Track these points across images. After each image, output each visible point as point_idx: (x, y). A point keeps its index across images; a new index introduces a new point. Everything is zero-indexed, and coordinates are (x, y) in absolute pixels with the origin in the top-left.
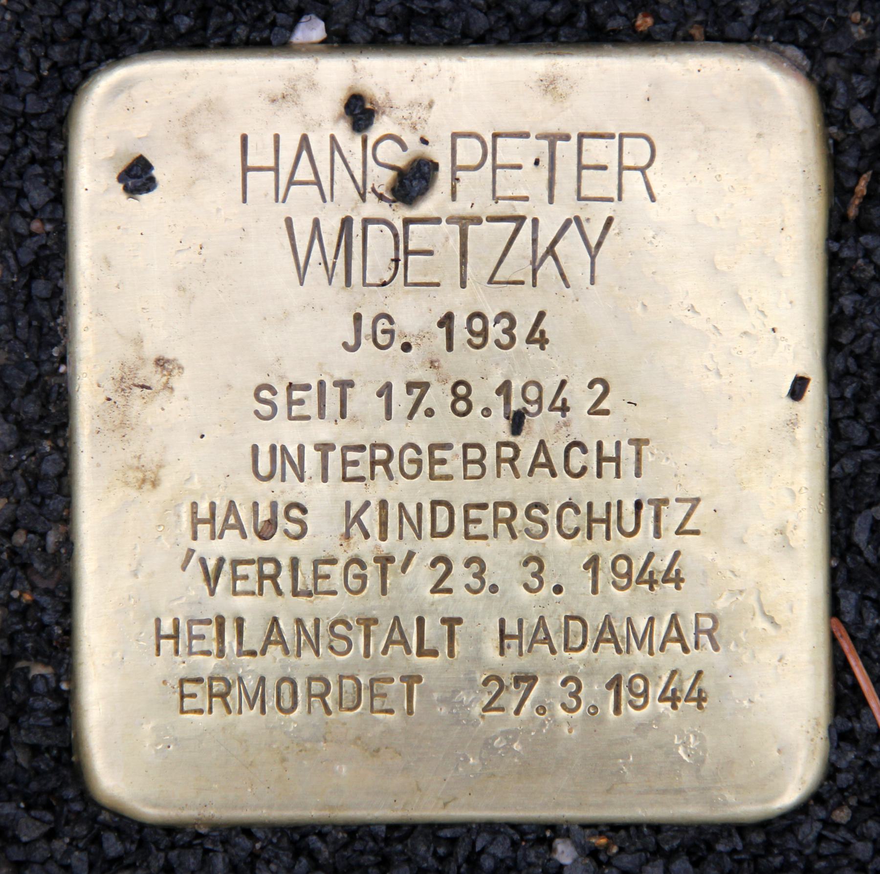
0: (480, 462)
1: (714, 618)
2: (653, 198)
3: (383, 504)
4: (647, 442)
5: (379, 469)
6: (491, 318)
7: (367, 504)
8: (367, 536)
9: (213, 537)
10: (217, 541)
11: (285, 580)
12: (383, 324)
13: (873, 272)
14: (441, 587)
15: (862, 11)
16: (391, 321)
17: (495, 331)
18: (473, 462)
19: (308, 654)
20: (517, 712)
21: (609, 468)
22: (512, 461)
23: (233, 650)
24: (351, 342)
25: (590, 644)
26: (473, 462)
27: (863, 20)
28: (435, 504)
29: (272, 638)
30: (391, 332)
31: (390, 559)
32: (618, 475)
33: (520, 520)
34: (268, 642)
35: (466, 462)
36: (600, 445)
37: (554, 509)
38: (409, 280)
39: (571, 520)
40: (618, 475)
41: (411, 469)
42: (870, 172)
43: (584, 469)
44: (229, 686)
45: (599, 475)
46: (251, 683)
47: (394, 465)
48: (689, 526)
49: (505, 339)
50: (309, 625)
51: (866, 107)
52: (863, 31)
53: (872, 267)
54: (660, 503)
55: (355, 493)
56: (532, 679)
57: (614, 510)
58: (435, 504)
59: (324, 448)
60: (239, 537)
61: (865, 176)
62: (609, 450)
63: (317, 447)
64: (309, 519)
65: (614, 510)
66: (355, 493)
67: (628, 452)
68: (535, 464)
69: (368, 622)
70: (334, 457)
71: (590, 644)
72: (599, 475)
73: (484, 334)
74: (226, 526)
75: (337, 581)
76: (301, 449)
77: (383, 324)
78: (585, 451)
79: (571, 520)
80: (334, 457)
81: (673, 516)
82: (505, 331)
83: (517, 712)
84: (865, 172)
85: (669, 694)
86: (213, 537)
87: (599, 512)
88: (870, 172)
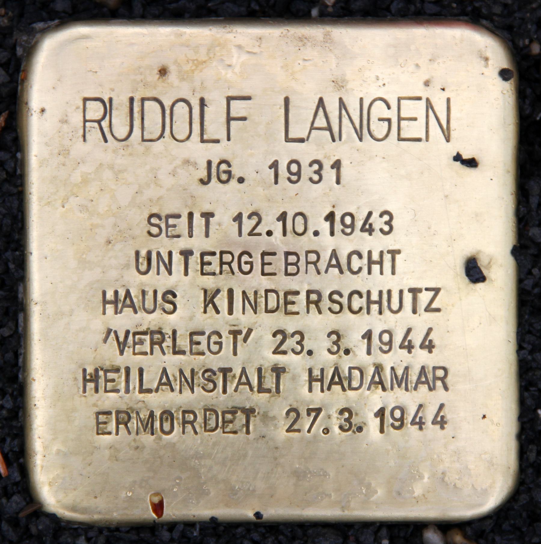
0: (296, 264)
1: (445, 369)
2: (248, 98)
3: (231, 292)
4: (399, 252)
5: (225, 267)
6: (305, 164)
7: (218, 291)
8: (218, 312)
9: (116, 313)
10: (119, 315)
11: (168, 342)
12: (224, 167)
13: (5, 176)
14: (279, 350)
15: (6, 8)
16: (229, 165)
17: (307, 172)
18: (292, 264)
19: (187, 392)
20: (309, 431)
21: (376, 268)
22: (315, 263)
23: (283, 383)
24: (206, 180)
25: (365, 386)
26: (292, 264)
27: (6, 14)
28: (267, 291)
29: (163, 381)
30: (229, 173)
31: (240, 332)
32: (382, 273)
33: (326, 303)
34: (160, 384)
35: (287, 264)
36: (370, 253)
37: (346, 294)
38: (291, 136)
39: (357, 303)
40: (382, 273)
41: (246, 268)
42: (7, 112)
43: (360, 269)
44: (129, 418)
45: (369, 273)
46: (144, 415)
47: (235, 265)
48: (434, 306)
49: (386, 228)
50: (188, 374)
51: (4, 70)
52: (6, 21)
53: (5, 173)
54: (414, 291)
55: (209, 282)
56: (318, 411)
57: (385, 296)
58: (267, 291)
59: (186, 254)
60: (132, 313)
61: (3, 114)
62: (375, 257)
63: (182, 253)
64: (177, 301)
65: (385, 296)
66: (209, 282)
67: (387, 257)
68: (330, 265)
69: (225, 371)
70: (194, 261)
71: (365, 386)
72: (369, 273)
73: (298, 174)
74: (124, 306)
75: (203, 347)
76: (170, 254)
77: (224, 167)
78: (360, 256)
79: (357, 303)
80: (194, 261)
81: (424, 298)
82: (316, 172)
83: (309, 431)
84: (4, 112)
85: (417, 420)
86: (116, 313)
87: (375, 297)
88: (7, 112)
